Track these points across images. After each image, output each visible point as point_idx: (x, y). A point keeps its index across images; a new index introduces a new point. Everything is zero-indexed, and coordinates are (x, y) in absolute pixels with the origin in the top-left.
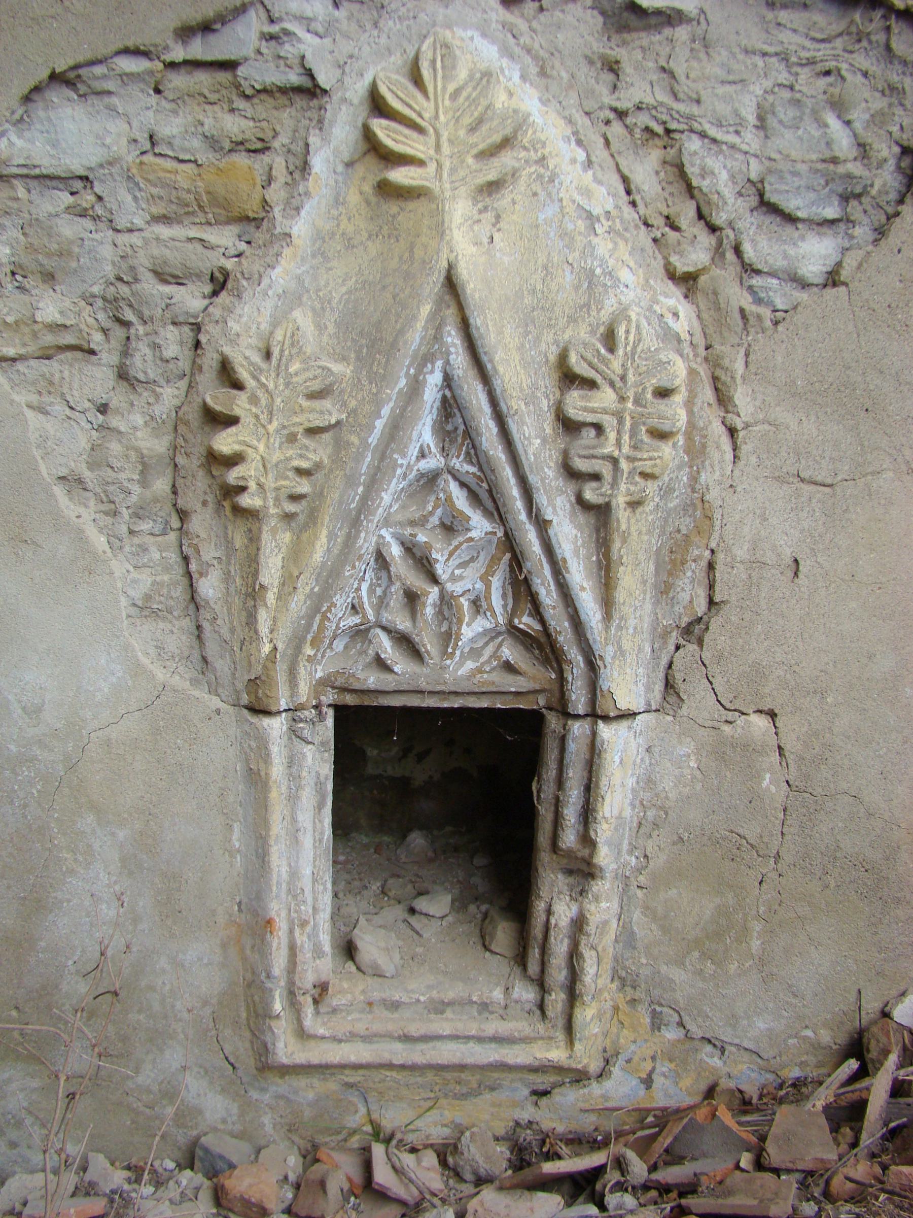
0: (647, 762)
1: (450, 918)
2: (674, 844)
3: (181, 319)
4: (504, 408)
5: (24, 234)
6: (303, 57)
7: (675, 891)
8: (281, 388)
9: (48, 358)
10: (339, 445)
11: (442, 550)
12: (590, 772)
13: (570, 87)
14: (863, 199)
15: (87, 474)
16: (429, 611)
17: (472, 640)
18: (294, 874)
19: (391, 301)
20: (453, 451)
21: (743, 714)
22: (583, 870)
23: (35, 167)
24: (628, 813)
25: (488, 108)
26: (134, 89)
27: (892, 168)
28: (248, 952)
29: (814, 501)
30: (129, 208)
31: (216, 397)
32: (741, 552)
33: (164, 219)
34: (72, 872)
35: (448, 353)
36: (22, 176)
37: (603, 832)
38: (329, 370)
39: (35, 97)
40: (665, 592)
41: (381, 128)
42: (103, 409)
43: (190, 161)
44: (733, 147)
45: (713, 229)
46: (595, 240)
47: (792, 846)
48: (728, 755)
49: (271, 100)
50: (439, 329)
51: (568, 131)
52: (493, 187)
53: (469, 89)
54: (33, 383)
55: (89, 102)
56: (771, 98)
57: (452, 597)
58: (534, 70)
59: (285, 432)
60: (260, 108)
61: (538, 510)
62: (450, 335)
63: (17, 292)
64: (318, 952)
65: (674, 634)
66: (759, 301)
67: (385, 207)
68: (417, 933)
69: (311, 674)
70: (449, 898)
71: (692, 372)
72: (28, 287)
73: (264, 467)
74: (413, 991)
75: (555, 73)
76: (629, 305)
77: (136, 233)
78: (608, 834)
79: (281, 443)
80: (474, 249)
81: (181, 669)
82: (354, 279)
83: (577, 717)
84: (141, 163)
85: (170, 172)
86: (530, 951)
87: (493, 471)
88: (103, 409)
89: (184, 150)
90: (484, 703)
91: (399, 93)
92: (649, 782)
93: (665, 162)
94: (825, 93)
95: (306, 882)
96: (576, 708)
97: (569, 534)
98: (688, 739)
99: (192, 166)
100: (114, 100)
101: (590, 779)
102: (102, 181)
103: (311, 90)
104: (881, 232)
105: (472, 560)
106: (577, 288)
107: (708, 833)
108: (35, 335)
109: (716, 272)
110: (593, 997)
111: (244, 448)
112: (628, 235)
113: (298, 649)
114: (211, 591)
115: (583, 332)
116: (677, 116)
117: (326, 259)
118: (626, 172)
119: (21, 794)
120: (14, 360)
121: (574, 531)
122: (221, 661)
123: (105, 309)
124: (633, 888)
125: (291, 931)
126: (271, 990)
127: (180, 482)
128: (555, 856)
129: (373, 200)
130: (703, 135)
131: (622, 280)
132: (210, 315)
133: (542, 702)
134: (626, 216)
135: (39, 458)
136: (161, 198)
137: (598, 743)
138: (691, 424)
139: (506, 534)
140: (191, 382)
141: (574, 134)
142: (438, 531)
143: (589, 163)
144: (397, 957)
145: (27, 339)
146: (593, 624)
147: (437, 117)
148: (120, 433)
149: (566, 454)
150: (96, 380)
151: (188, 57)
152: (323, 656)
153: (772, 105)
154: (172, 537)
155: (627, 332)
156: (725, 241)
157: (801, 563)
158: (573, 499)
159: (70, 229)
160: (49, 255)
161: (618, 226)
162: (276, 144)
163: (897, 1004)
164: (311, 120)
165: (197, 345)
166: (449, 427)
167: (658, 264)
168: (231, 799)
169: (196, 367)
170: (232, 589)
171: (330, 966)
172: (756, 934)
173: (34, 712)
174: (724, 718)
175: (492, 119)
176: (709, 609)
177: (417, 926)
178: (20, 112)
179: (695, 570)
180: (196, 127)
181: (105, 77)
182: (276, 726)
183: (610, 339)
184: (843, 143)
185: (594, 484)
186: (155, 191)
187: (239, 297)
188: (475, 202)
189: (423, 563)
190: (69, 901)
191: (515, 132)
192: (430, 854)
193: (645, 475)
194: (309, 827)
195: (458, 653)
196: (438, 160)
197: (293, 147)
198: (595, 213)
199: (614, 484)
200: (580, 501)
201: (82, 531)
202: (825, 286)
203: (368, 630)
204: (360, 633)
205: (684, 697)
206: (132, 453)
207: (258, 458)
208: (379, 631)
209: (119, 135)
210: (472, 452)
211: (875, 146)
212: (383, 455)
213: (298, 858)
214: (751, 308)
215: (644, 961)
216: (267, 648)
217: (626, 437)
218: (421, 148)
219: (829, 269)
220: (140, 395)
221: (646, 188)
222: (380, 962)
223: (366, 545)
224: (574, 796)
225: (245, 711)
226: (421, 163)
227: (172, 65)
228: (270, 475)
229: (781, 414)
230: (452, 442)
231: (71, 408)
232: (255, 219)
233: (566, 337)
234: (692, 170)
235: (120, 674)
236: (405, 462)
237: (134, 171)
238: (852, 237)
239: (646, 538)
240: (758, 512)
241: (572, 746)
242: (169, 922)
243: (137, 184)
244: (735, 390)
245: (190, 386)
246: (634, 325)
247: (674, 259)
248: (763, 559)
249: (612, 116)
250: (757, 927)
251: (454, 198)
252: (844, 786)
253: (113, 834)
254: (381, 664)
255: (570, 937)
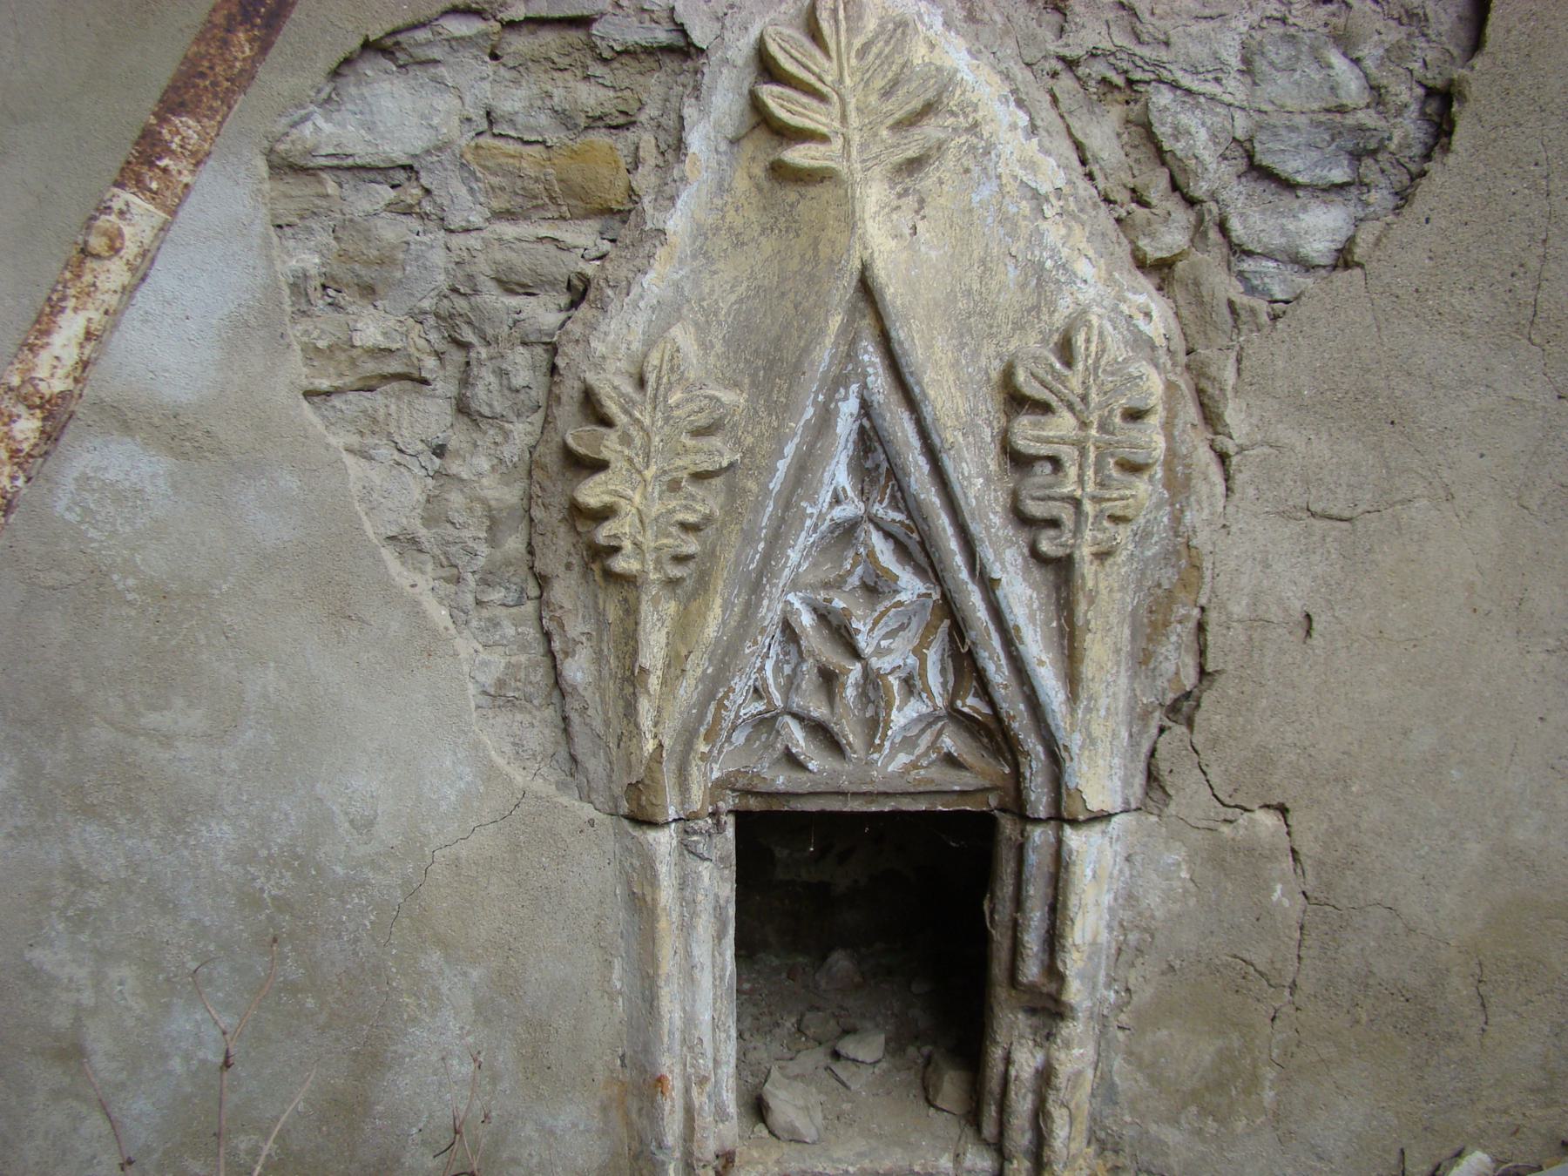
0: (1127, 874)
1: (884, 1065)
2: (1163, 973)
3: (532, 338)
4: (937, 441)
5: (336, 238)
6: (673, 9)
7: (1165, 1032)
8: (660, 423)
9: (371, 390)
10: (733, 492)
11: (865, 617)
12: (1056, 888)
13: (1007, 32)
14: (1380, 157)
15: (422, 532)
16: (850, 693)
17: (905, 728)
18: (690, 1021)
19: (792, 312)
20: (875, 494)
21: (1246, 810)
22: (1049, 1009)
23: (348, 156)
24: (1104, 937)
25: (904, 66)
26: (466, 56)
27: (1415, 115)
28: (634, 1116)
29: (1329, 539)
30: (465, 205)
31: (578, 437)
32: (1239, 608)
33: (508, 215)
34: (414, 1020)
35: (866, 375)
36: (331, 168)
37: (1074, 963)
38: (718, 400)
39: (345, 70)
40: (1145, 662)
41: (771, 95)
42: (440, 451)
43: (537, 142)
44: (1212, 98)
45: (1191, 202)
46: (1044, 226)
47: (1312, 973)
48: (1227, 862)
49: (634, 64)
50: (853, 344)
51: (1006, 90)
52: (914, 165)
53: (881, 44)
54: (354, 421)
55: (411, 74)
56: (1258, 35)
57: (878, 675)
58: (960, 14)
59: (666, 478)
60: (621, 74)
61: (983, 566)
62: (866, 352)
63: (329, 309)
64: (721, 1114)
65: (1157, 714)
66: (1251, 290)
67: (780, 193)
68: (843, 1083)
69: (705, 774)
70: (882, 1038)
71: (1170, 386)
72: (343, 303)
73: (641, 521)
74: (839, 1160)
75: (986, 17)
76: (1089, 306)
77: (474, 234)
78: (1080, 964)
79: (661, 493)
80: (893, 243)
81: (544, 770)
82: (745, 285)
83: (1037, 821)
84: (477, 147)
85: (513, 157)
86: (985, 1108)
87: (925, 519)
88: (440, 451)
89: (532, 129)
90: (922, 806)
91: (793, 52)
92: (1129, 898)
93: (1128, 122)
94: (1326, 25)
95: (705, 1030)
96: (1037, 810)
97: (1022, 595)
98: (1178, 844)
99: (540, 148)
100: (442, 70)
101: (1055, 898)
102: (431, 171)
103: (684, 50)
104: (1403, 197)
105: (902, 627)
106: (1023, 286)
107: (1205, 959)
108: (353, 362)
109: (1197, 256)
110: (1065, 1166)
111: (615, 499)
112: (1085, 217)
113: (689, 745)
114: (579, 675)
115: (1032, 342)
116: (1141, 63)
117: (710, 260)
118: (1079, 136)
119: (351, 926)
120: (328, 394)
121: (1029, 592)
122: (593, 761)
123: (438, 328)
124: (1113, 1029)
125: (687, 1090)
126: (663, 1163)
127: (537, 540)
128: (1013, 993)
129: (766, 185)
130: (1174, 86)
131: (1080, 274)
132: (567, 333)
133: (993, 801)
134: (1081, 192)
135: (362, 514)
136: (502, 189)
137: (1065, 855)
138: (1171, 452)
139: (943, 595)
140: (547, 416)
141: (1013, 92)
142: (859, 593)
143: (1033, 129)
144: (819, 1116)
145: (343, 367)
146: (1055, 706)
147: (841, 80)
148: (462, 480)
149: (1015, 496)
150: (430, 415)
151: (530, 15)
152: (720, 753)
153: (1260, 43)
154: (530, 607)
155: (1088, 341)
156: (1207, 218)
157: (1315, 618)
158: (1026, 551)
159: (391, 231)
160: (368, 264)
161: (1072, 206)
162: (643, 117)
163: (1450, 1168)
164: (684, 86)
165: (554, 369)
166: (869, 464)
167: (1123, 251)
168: (610, 929)
169: (553, 398)
170: (605, 672)
171: (736, 1130)
172: (1268, 1084)
173: (365, 826)
174: (1222, 817)
175: (910, 80)
176: (1200, 681)
177: (843, 1076)
178: (328, 89)
179: (1181, 633)
180: (542, 99)
181: (429, 43)
182: (664, 841)
183: (1066, 350)
184: (1351, 86)
185: (1052, 533)
186: (495, 180)
187: (604, 310)
188: (893, 183)
189: (840, 633)
190: (412, 1056)
191: (940, 94)
192: (858, 979)
193: (1116, 519)
194: (708, 962)
195: (887, 744)
196: (844, 130)
197: (663, 121)
198: (1042, 191)
199: (1077, 532)
200: (1035, 553)
201: (418, 603)
202: (1335, 267)
203: (774, 718)
204: (766, 723)
205: (1171, 792)
206: (478, 506)
207: (634, 511)
208: (788, 719)
209: (449, 113)
210: (899, 495)
211: (1392, 89)
212: (788, 502)
213: (694, 1000)
214: (1242, 300)
215: (1128, 1119)
216: (650, 746)
217: (1090, 473)
218: (823, 119)
219: (1340, 246)
220: (485, 433)
221: (1105, 155)
222: (797, 1124)
223: (770, 615)
224: (1036, 917)
225: (626, 822)
226: (824, 139)
227: (511, 25)
228: (649, 532)
229: (1284, 433)
230: (874, 482)
231: (400, 451)
232: (619, 211)
233: (1012, 348)
234: (1163, 129)
235: (470, 779)
236: (815, 511)
237: (469, 157)
238: (1367, 204)
239: (1118, 596)
240: (1259, 556)
241: (1032, 858)
242: (535, 1081)
243: (473, 173)
244: (1226, 406)
245: (546, 421)
246: (1096, 332)
247: (1143, 243)
248: (1267, 617)
249: (1059, 66)
250: (1270, 1073)
251: (866, 181)
252: (1377, 895)
253: (465, 974)
254: (792, 760)
255: (1034, 1092)
